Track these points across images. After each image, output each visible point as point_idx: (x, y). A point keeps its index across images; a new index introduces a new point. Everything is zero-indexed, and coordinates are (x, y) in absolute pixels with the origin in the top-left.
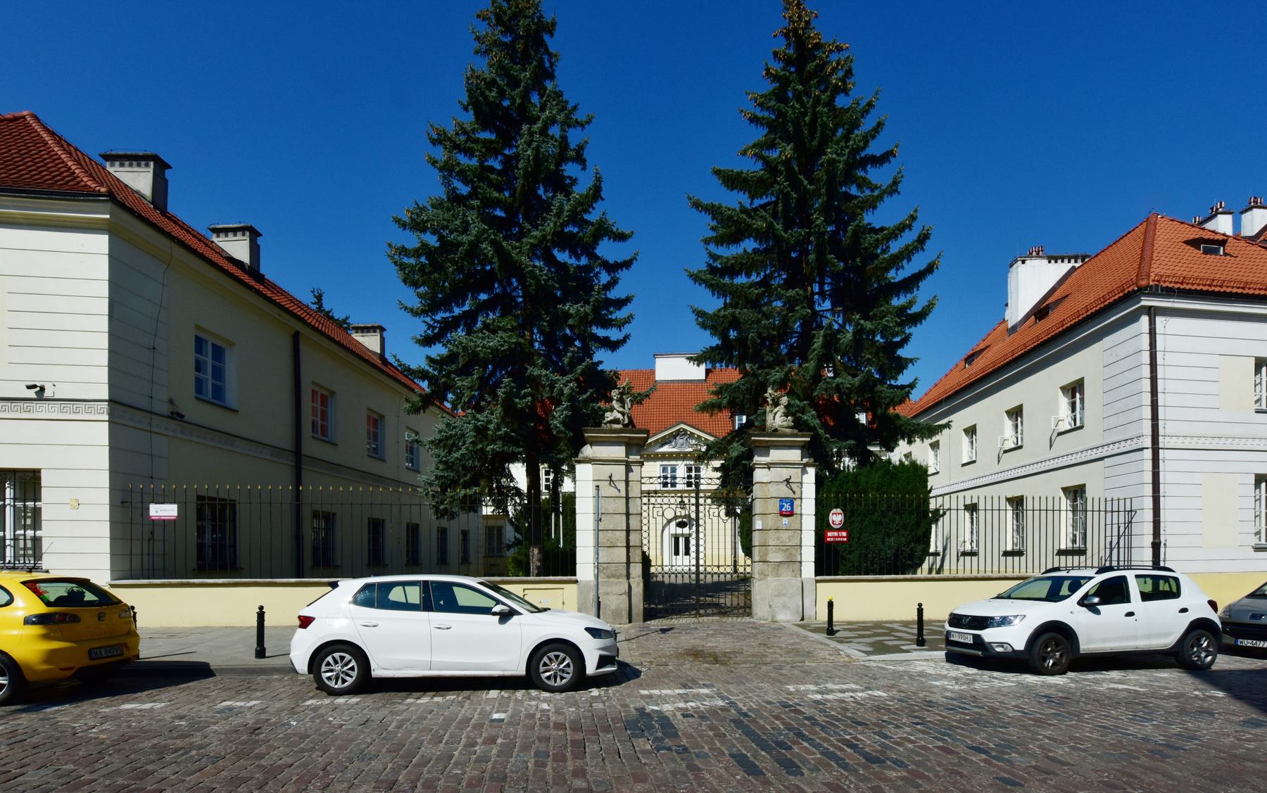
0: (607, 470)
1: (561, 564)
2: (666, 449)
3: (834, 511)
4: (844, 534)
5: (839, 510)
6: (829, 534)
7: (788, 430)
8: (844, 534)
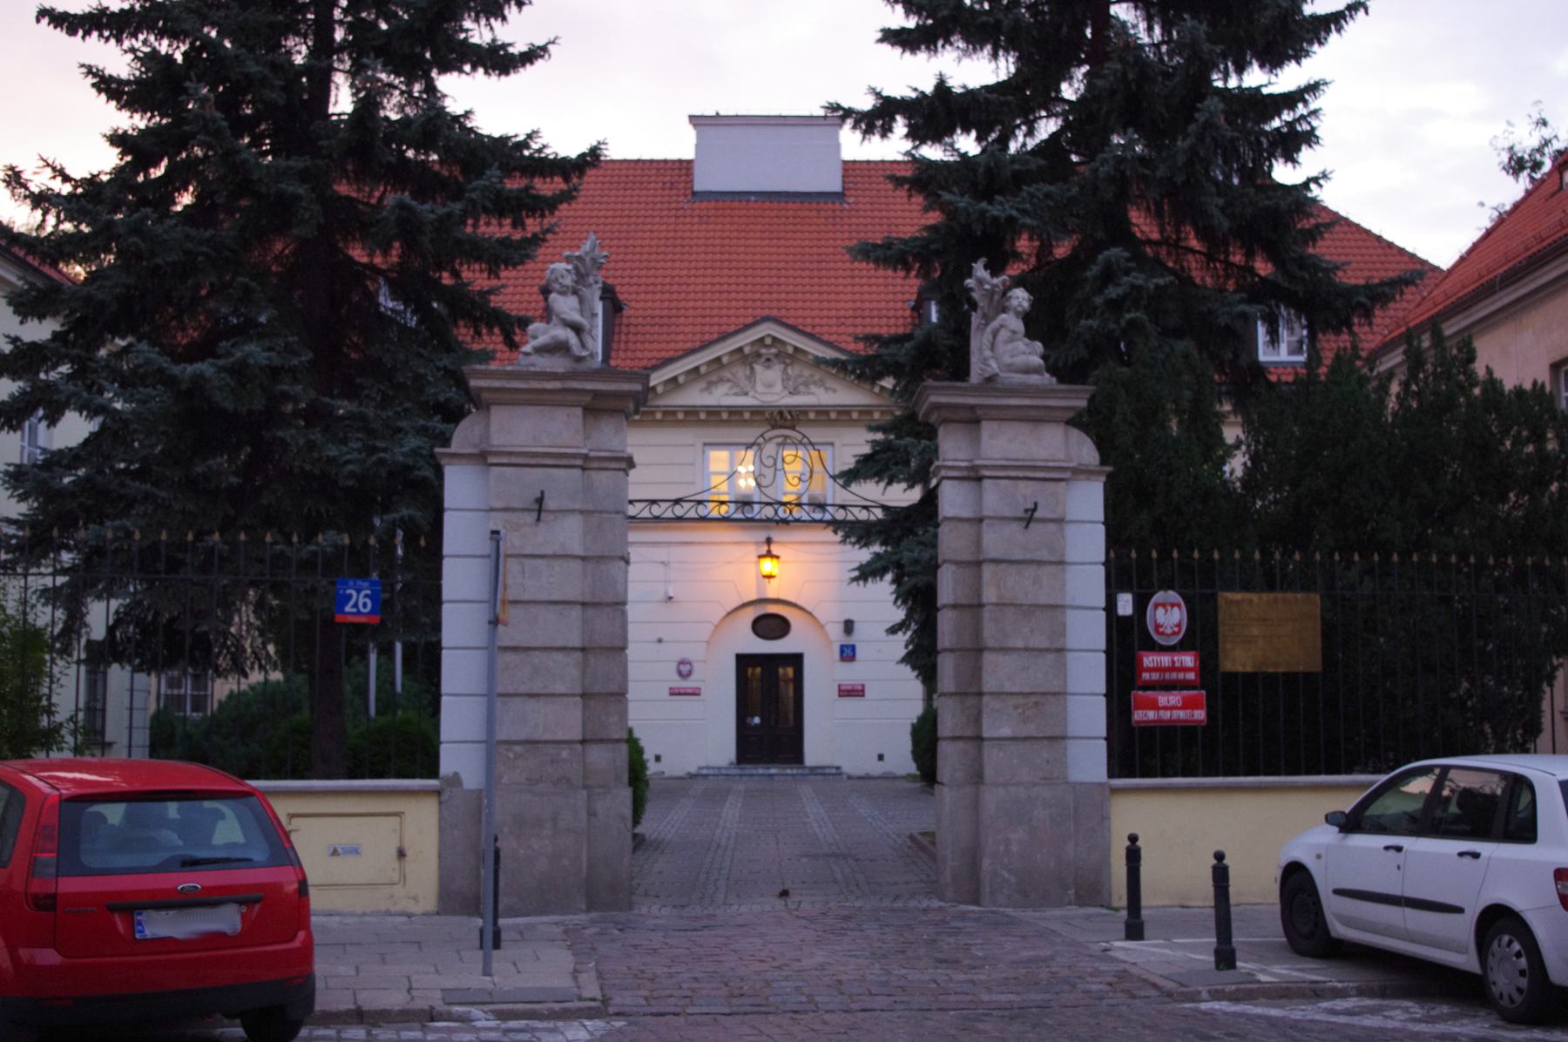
0: (535, 479)
1: (407, 750)
3: (1160, 596)
4: (1188, 660)
5: (1173, 596)
6: (1149, 660)
7: (1034, 379)
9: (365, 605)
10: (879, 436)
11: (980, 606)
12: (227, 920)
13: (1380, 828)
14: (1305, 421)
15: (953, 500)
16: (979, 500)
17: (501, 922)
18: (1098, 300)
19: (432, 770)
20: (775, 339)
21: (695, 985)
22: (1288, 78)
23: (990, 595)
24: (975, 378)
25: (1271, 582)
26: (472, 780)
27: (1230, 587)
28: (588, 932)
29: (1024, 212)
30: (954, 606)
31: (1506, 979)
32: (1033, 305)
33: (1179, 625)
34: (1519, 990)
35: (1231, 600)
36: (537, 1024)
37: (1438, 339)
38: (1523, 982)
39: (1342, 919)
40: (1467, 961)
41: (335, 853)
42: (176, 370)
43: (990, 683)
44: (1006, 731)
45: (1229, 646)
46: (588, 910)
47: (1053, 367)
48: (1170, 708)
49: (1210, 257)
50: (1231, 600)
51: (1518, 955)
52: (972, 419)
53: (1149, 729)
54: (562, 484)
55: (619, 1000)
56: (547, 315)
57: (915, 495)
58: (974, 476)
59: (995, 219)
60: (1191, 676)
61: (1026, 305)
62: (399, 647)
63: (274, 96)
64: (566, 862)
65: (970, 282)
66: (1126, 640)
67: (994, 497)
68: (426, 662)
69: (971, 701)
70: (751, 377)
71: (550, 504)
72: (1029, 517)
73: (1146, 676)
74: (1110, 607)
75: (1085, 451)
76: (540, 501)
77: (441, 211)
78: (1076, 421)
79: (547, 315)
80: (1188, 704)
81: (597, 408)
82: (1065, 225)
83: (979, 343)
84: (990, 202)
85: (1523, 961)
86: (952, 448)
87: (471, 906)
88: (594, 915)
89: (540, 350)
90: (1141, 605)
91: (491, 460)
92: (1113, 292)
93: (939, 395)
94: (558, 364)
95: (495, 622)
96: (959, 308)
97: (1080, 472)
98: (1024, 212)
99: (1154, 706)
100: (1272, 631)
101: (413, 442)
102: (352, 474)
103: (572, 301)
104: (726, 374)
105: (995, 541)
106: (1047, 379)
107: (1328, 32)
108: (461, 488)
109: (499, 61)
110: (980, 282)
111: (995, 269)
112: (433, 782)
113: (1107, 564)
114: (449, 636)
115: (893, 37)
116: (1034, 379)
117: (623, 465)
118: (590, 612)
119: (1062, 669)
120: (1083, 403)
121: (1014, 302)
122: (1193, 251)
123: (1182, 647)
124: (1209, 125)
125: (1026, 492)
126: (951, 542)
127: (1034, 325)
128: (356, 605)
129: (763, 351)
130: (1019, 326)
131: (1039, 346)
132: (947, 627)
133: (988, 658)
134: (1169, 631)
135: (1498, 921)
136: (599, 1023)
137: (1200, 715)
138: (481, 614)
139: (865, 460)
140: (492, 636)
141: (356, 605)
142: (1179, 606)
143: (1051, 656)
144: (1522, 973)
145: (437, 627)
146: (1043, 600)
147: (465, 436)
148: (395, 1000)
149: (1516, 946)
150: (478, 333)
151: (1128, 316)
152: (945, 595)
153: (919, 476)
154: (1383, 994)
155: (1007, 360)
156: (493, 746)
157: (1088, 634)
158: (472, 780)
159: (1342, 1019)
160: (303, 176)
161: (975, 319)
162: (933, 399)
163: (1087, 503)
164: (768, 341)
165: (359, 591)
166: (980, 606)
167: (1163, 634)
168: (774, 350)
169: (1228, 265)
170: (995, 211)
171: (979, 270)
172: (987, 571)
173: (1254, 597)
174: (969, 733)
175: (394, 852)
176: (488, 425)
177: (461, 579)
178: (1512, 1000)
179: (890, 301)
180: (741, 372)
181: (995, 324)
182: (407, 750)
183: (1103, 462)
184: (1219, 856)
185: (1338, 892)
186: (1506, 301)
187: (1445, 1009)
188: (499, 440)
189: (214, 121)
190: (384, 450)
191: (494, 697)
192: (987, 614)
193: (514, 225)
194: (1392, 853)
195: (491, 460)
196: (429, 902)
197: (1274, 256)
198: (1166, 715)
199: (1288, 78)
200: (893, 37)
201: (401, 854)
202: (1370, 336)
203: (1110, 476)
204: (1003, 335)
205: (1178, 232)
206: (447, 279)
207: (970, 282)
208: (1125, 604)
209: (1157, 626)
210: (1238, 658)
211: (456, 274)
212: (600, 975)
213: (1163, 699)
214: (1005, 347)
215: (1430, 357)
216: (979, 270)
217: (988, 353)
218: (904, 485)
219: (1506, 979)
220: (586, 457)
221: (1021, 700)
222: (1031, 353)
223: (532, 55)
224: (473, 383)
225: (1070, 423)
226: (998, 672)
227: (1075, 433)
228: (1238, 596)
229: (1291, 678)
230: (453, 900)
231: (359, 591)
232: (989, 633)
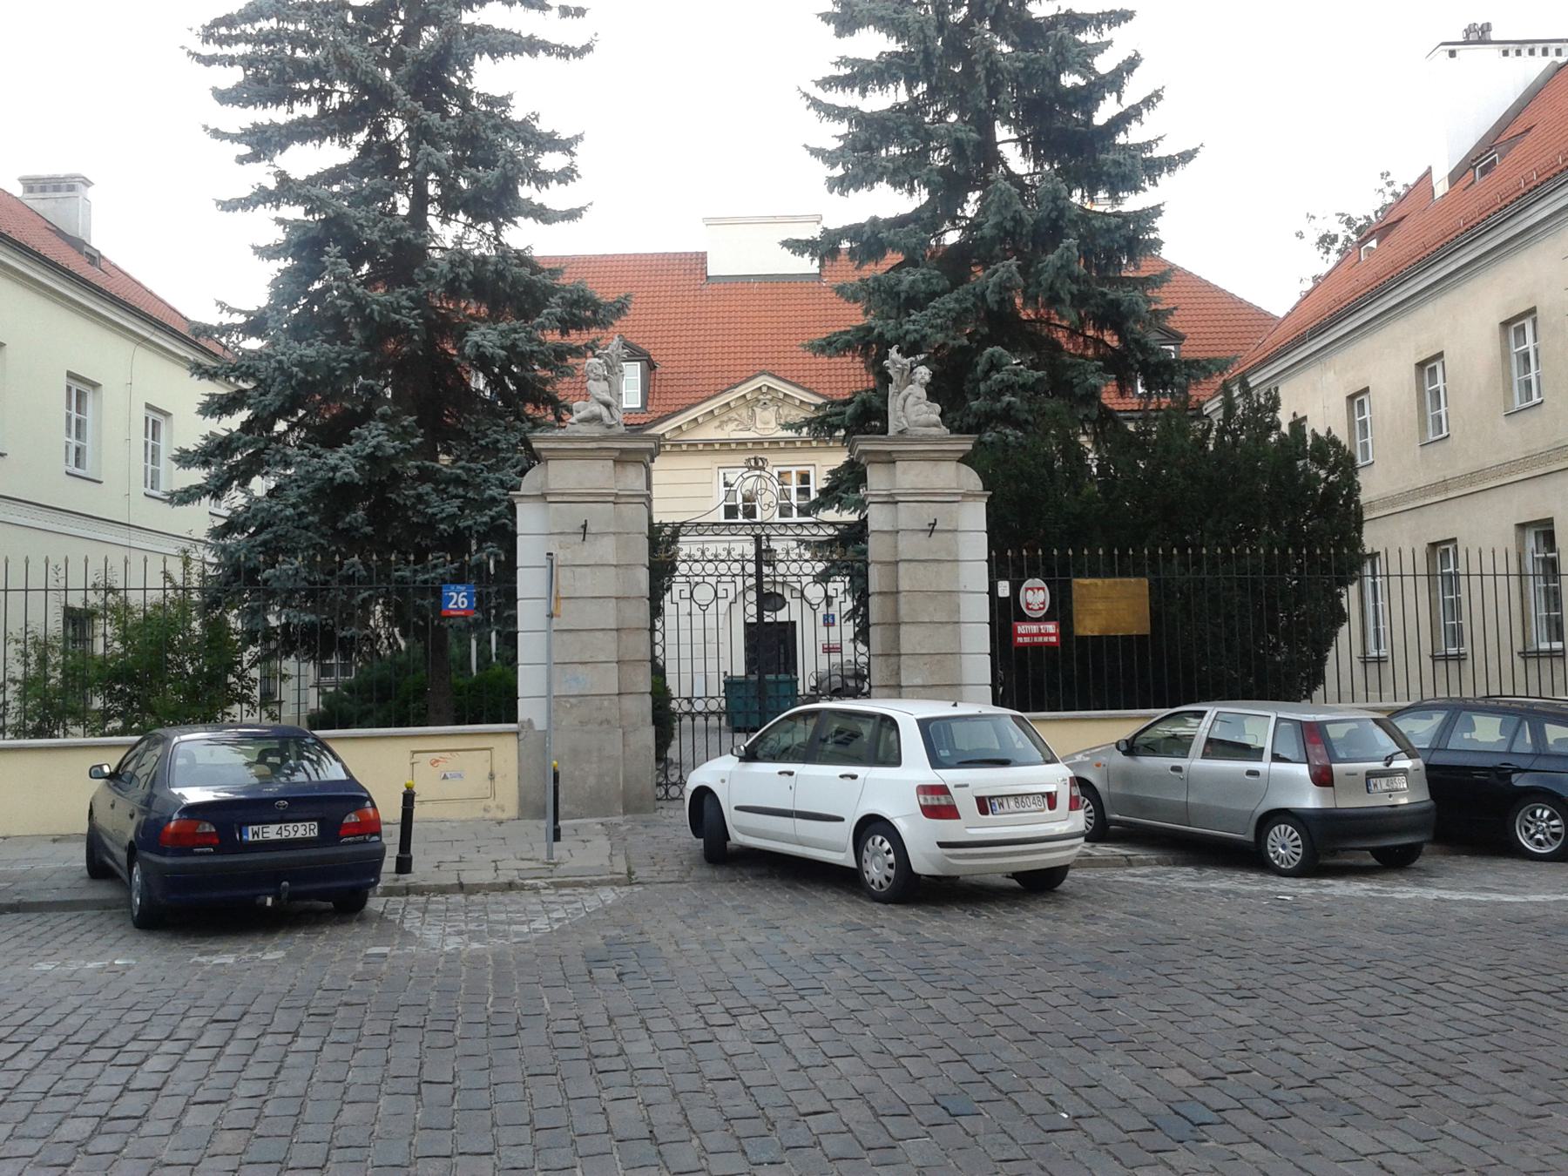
0: (581, 512)
1: (492, 701)
3: (1029, 583)
4: (1051, 628)
5: (1039, 582)
6: (1022, 628)
7: (934, 431)
11: (898, 592)
12: (305, 830)
13: (773, 758)
15: (878, 518)
16: (896, 518)
17: (560, 823)
22: (1132, 203)
23: (904, 585)
24: (891, 432)
26: (540, 724)
27: (1080, 574)
28: (622, 828)
30: (880, 593)
31: (877, 870)
32: (933, 377)
34: (888, 879)
35: (1080, 583)
36: (581, 890)
37: (1246, 391)
38: (891, 873)
39: (743, 831)
40: (846, 858)
41: (445, 777)
43: (905, 647)
44: (918, 681)
46: (625, 813)
50: (1080, 583)
51: (888, 852)
52: (889, 459)
54: (598, 515)
55: (641, 873)
56: (586, 395)
58: (891, 501)
61: (927, 378)
62: (493, 635)
64: (607, 779)
66: (1004, 615)
67: (907, 516)
68: (510, 640)
69: (893, 660)
70: (753, 416)
71: (591, 528)
72: (932, 529)
73: (1020, 640)
74: (993, 591)
76: (585, 527)
78: (966, 459)
79: (586, 395)
81: (623, 459)
83: (894, 405)
85: (891, 857)
86: (877, 480)
87: (539, 813)
88: (629, 816)
89: (581, 421)
90: (1015, 590)
91: (549, 499)
93: (866, 445)
94: (595, 430)
95: (551, 616)
100: (1112, 605)
103: (604, 385)
104: (733, 415)
107: (1162, 170)
108: (528, 519)
109: (542, 214)
110: (894, 362)
112: (513, 726)
113: (989, 561)
114: (522, 625)
115: (242, 160)
116: (934, 431)
118: (622, 603)
119: (957, 637)
120: (970, 447)
121: (918, 376)
123: (1047, 618)
125: (928, 513)
126: (876, 548)
127: (933, 392)
130: (924, 394)
131: (938, 408)
133: (903, 628)
135: (871, 826)
136: (626, 889)
138: (542, 608)
140: (550, 624)
143: (949, 627)
144: (891, 866)
145: (514, 619)
146: (944, 587)
147: (530, 483)
148: (486, 877)
149: (887, 845)
152: (874, 586)
153: (861, 505)
154: (1175, 864)
155: (913, 418)
156: (554, 701)
157: (977, 610)
158: (540, 724)
159: (1137, 880)
161: (892, 388)
162: (861, 447)
163: (975, 516)
166: (898, 592)
172: (902, 567)
173: (1099, 581)
174: (892, 682)
175: (487, 774)
176: (546, 476)
177: (529, 583)
178: (881, 886)
179: (850, 376)
180: (744, 412)
181: (905, 393)
182: (492, 701)
183: (985, 489)
185: (737, 808)
186: (147, 335)
188: (555, 484)
191: (553, 665)
192: (902, 598)
193: (562, 334)
194: (785, 777)
195: (549, 499)
196: (512, 810)
197: (1118, 329)
199: (1132, 203)
200: (242, 160)
201: (492, 777)
203: (990, 498)
204: (911, 400)
208: (1004, 589)
210: (1088, 625)
212: (627, 858)
214: (912, 406)
215: (1239, 401)
217: (900, 413)
219: (877, 870)
220: (617, 495)
222: (932, 412)
223: (572, 215)
224: (535, 445)
225: (960, 461)
226: (910, 639)
227: (965, 468)
228: (1087, 581)
229: (1127, 639)
230: (528, 808)
232: (904, 612)
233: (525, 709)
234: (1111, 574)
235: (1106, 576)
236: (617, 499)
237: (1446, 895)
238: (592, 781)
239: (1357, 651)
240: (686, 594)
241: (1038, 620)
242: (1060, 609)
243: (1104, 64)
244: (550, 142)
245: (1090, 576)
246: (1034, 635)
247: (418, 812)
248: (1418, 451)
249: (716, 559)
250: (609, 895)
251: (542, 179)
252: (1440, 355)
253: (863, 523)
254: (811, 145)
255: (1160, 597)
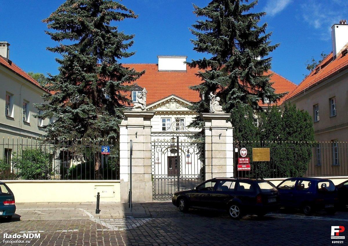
2: (159, 109)
3: (242, 149)
4: (247, 160)
5: (244, 149)
6: (240, 160)
7: (221, 112)
8: (247, 160)
9: (107, 151)
10: (194, 119)
12: (265, 179)
14: (271, 117)
15: (207, 132)
18: (232, 97)
19: (118, 178)
20: (174, 98)
21: (165, 213)
25: (262, 145)
29: (219, 82)
33: (246, 154)
42: (73, 111)
45: (254, 157)
47: (224, 109)
48: (244, 168)
49: (252, 89)
52: (209, 120)
53: (240, 171)
54: (140, 130)
57: (201, 130)
59: (214, 83)
60: (248, 162)
61: (219, 100)
63: (88, 63)
65: (210, 96)
66: (237, 156)
72: (220, 136)
73: (240, 162)
74: (234, 150)
75: (229, 124)
76: (136, 134)
77: (117, 83)
80: (247, 167)
82: (226, 84)
84: (213, 80)
90: (239, 150)
92: (235, 96)
94: (140, 110)
96: (208, 100)
97: (227, 128)
98: (219, 82)
99: (242, 167)
101: (113, 122)
102: (103, 128)
105: (216, 139)
106: (223, 112)
108: (123, 131)
109: (127, 55)
110: (211, 96)
111: (213, 93)
117: (151, 127)
122: (249, 87)
124: (251, 68)
125: (219, 131)
126: (208, 140)
127: (221, 103)
128: (105, 151)
129: (172, 100)
130: (218, 103)
132: (207, 154)
134: (244, 155)
137: (249, 169)
139: (191, 124)
141: (105, 151)
142: (246, 150)
143: (224, 159)
150: (123, 102)
151: (237, 100)
157: (231, 155)
160: (93, 77)
164: (173, 99)
165: (106, 149)
167: (243, 155)
168: (174, 100)
169: (255, 90)
170: (213, 82)
171: (211, 94)
173: (259, 149)
184: (99, 193)
187: (285, 215)
189: (79, 69)
190: (108, 124)
198: (243, 169)
202: (280, 103)
205: (246, 84)
206: (117, 93)
207: (210, 96)
208: (236, 150)
209: (242, 154)
210: (256, 159)
211: (119, 92)
213: (243, 166)
214: (216, 107)
216: (211, 94)
218: (198, 128)
221: (218, 166)
226: (215, 162)
231: (106, 149)
233: (121, 176)
234: (262, 147)
235: (260, 147)
236: (144, 127)
237: (337, 219)
238: (138, 194)
239: (331, 164)
240: (160, 150)
241: (243, 158)
242: (250, 155)
243: (260, 25)
244: (127, 38)
245: (257, 147)
246: (243, 161)
247: (101, 200)
248: (329, 119)
249: (161, 142)
250: (144, 221)
251: (126, 47)
252: (335, 97)
253: (203, 132)
254: (133, 19)
255: (273, 152)
